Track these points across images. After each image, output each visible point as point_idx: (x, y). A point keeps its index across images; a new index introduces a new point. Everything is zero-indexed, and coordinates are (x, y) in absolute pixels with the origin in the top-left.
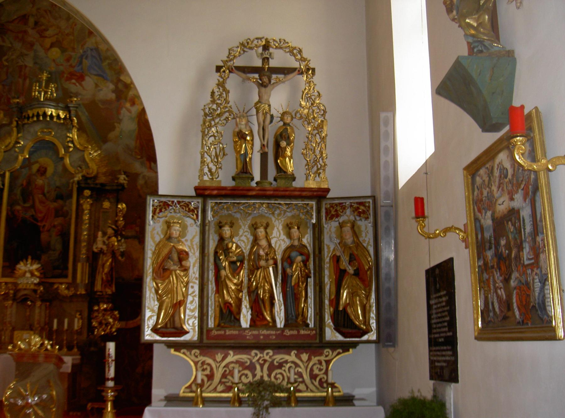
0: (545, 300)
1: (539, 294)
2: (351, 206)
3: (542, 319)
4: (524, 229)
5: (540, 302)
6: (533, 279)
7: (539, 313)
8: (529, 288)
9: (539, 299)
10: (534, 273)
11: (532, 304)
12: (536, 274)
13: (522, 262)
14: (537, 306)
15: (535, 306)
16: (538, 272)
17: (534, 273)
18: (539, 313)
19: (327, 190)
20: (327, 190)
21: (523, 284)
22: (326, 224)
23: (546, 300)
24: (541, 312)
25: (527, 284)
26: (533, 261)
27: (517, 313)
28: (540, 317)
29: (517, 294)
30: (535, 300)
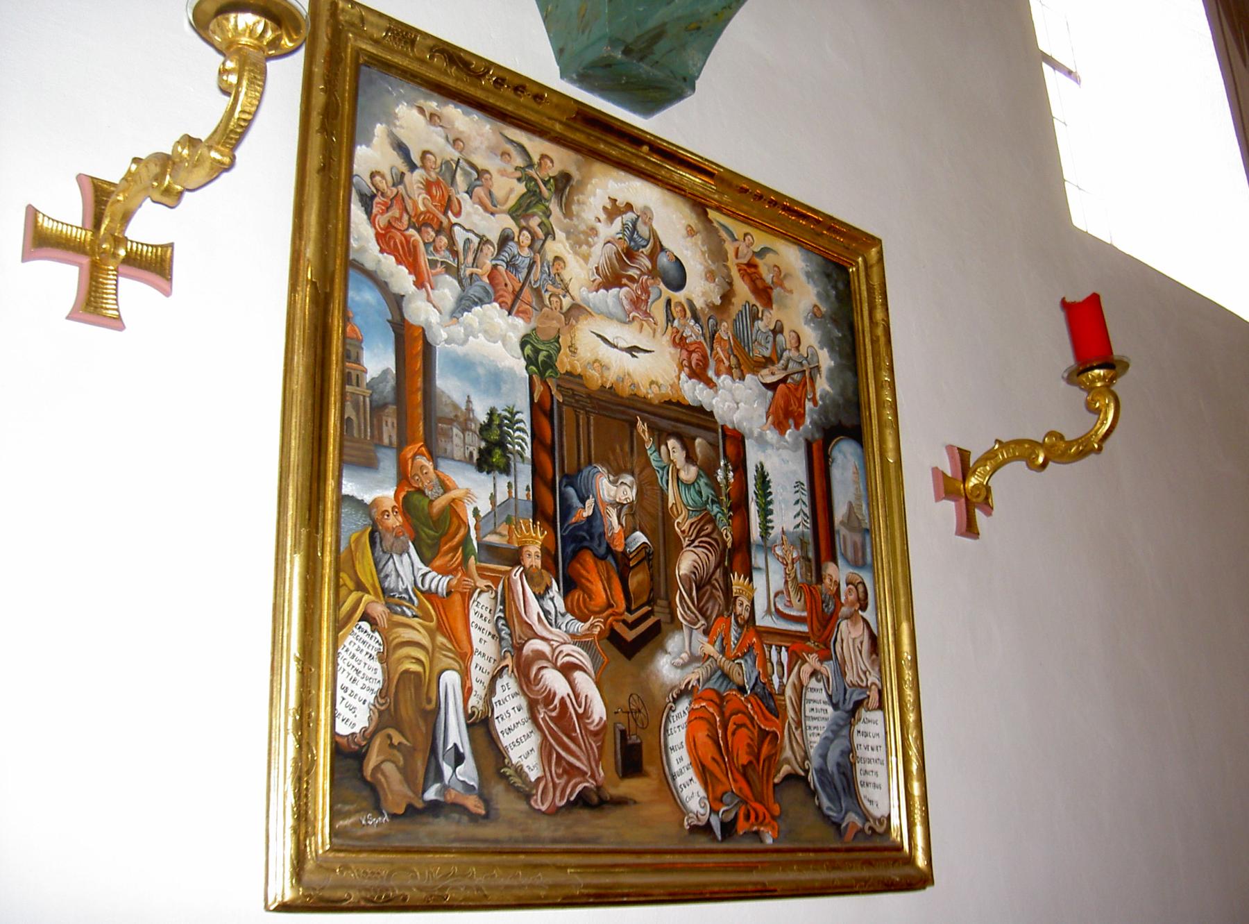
0: (853, 765)
1: (827, 742)
2: (435, 249)
3: (837, 825)
4: (765, 512)
5: (831, 767)
6: (800, 689)
7: (826, 803)
8: (777, 711)
9: (824, 757)
10: (807, 669)
11: (786, 769)
12: (814, 673)
13: (741, 609)
14: (812, 778)
15: (805, 779)
16: (828, 668)
17: (807, 669)
18: (826, 803)
19: (936, 471)
20: (936, 471)
21: (742, 689)
22: (512, 418)
23: (859, 766)
24: (835, 798)
25: (768, 699)
26: (804, 628)
27: (693, 794)
28: (827, 818)
29: (695, 717)
30: (806, 757)
